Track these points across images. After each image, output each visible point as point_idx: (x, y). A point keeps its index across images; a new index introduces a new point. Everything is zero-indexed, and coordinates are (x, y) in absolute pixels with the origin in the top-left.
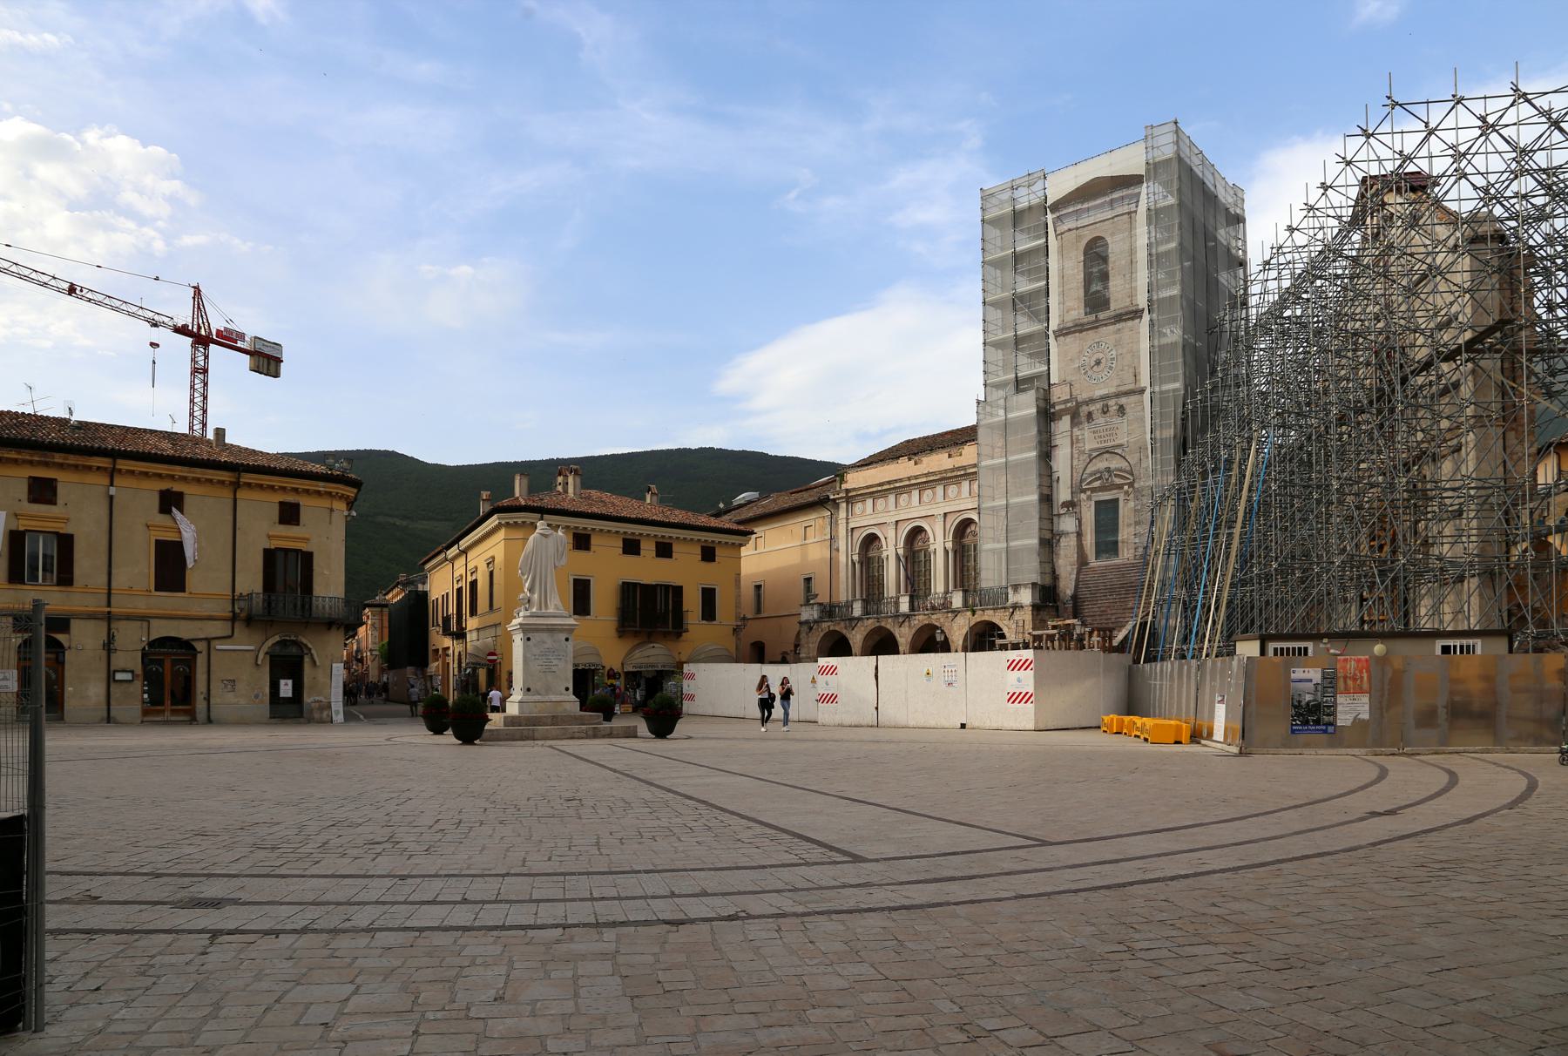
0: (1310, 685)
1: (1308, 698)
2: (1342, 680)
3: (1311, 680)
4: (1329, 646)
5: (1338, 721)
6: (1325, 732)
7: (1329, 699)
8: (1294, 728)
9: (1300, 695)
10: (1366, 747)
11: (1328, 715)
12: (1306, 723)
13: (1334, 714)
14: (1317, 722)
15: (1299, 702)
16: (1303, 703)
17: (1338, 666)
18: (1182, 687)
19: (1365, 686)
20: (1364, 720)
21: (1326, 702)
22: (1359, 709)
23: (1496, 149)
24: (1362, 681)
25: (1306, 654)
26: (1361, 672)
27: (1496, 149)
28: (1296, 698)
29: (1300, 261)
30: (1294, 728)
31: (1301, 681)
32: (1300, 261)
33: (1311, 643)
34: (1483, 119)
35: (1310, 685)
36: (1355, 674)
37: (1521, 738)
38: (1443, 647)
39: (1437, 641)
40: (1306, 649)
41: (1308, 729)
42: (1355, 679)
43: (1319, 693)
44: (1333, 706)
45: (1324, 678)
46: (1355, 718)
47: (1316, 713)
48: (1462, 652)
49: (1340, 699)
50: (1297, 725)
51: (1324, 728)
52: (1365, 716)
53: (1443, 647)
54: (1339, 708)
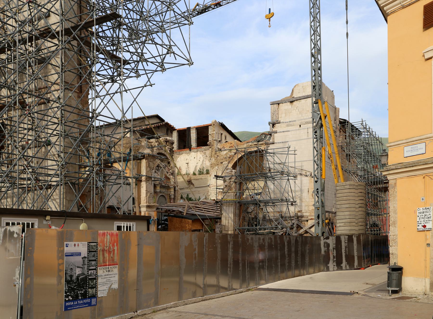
0: (79, 259)
1: (78, 271)
2: (101, 253)
3: (79, 254)
4: (50, 223)
5: (99, 293)
6: (90, 304)
7: (92, 271)
8: (67, 304)
9: (71, 269)
10: (117, 315)
11: (92, 288)
12: (76, 298)
13: (95, 287)
14: (84, 296)
15: (71, 276)
16: (74, 278)
17: (99, 240)
18: (227, 250)
19: (116, 258)
20: (115, 289)
21: (91, 275)
22: (112, 279)
23: (162, 49)
24: (114, 254)
25: (33, 226)
26: (113, 245)
27: (162, 49)
28: (69, 272)
29: (147, 72)
30: (67, 304)
31: (72, 255)
32: (147, 72)
33: (37, 219)
34: (285, 163)
35: (79, 259)
36: (110, 247)
37: (265, 273)
38: (118, 226)
39: (115, 222)
40: (33, 224)
41: (78, 304)
42: (110, 252)
43: (86, 267)
44: (95, 279)
45: (89, 251)
46: (110, 288)
47: (83, 287)
48: (127, 230)
49: (100, 272)
50: (69, 301)
51: (88, 300)
52: (115, 286)
53: (118, 226)
54: (100, 280)
